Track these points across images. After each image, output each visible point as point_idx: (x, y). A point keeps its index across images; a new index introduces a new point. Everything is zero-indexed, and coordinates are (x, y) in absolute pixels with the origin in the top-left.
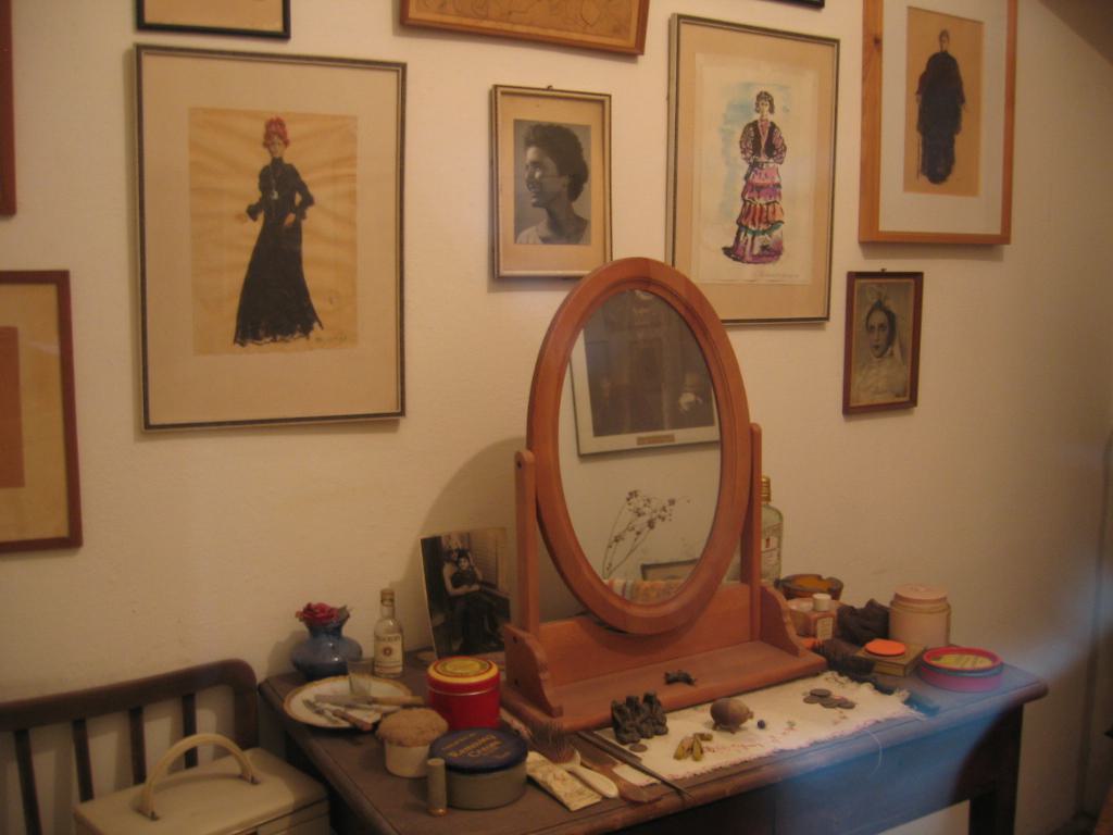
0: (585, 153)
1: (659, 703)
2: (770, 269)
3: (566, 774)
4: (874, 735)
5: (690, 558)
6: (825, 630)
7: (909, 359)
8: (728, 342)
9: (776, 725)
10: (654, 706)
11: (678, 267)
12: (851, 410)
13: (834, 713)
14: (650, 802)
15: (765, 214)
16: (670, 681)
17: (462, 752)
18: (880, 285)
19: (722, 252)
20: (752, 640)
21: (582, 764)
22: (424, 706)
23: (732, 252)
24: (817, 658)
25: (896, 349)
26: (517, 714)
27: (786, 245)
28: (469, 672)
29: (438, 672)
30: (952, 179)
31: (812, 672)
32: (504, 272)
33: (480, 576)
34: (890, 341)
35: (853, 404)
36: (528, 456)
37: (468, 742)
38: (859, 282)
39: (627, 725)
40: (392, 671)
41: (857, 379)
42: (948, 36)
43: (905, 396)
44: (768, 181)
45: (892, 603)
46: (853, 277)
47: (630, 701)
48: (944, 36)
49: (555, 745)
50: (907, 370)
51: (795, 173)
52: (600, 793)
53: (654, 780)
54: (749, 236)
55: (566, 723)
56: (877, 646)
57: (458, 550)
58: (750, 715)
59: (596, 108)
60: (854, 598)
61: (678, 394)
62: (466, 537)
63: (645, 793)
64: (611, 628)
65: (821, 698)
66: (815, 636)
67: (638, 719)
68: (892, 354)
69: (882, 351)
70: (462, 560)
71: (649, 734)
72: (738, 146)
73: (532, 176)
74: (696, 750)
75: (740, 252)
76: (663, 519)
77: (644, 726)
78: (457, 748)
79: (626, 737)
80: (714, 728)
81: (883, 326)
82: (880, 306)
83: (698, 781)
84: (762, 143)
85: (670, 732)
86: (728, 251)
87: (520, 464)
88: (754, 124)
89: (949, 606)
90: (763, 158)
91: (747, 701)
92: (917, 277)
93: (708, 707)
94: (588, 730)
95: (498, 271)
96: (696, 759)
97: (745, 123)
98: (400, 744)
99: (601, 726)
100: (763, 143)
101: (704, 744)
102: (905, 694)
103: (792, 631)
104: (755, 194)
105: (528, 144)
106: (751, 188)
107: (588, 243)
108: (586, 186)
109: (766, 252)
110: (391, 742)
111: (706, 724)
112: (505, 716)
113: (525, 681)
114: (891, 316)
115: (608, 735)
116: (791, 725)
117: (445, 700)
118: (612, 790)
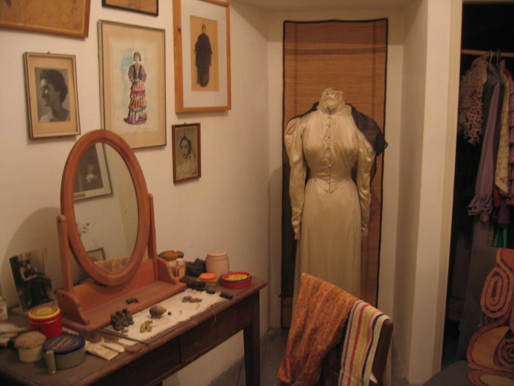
0: (66, 82)
1: (129, 312)
2: (142, 126)
3: (101, 347)
4: (212, 310)
5: (97, 248)
6: (182, 273)
7: (197, 157)
8: (135, 159)
9: (175, 313)
10: (127, 314)
11: (107, 128)
12: (176, 181)
13: (195, 304)
14: (138, 351)
15: (139, 103)
16: (129, 302)
17: (58, 346)
18: (184, 130)
19: (123, 121)
20: (155, 281)
21: (105, 342)
22: (30, 331)
23: (128, 120)
24: (183, 284)
25: (192, 155)
26: (69, 327)
27: (148, 116)
28: (47, 312)
29: (34, 315)
30: (209, 85)
31: (182, 290)
32: (35, 136)
33: (37, 271)
34: (189, 152)
35: (177, 179)
36: (63, 217)
37: (59, 342)
38: (177, 129)
39: (118, 323)
40: (4, 319)
41: (178, 169)
42: (205, 27)
43: (196, 173)
44: (140, 90)
45: (206, 258)
46: (174, 127)
47: (118, 313)
48: (203, 27)
49: (94, 336)
50: (196, 163)
51: (149, 85)
52: (117, 351)
53: (136, 342)
54: (134, 113)
55: (93, 326)
56: (203, 276)
57: (25, 261)
58: (165, 311)
59: (69, 62)
60: (190, 258)
61: (86, 174)
62: (29, 255)
63: (135, 347)
64: (102, 285)
65: (188, 299)
66: (178, 275)
67: (121, 320)
68: (190, 157)
69: (186, 157)
70: (28, 265)
71: (127, 324)
72: (128, 75)
73: (44, 92)
74: (148, 328)
75: (131, 120)
76: (85, 232)
77: (125, 323)
78: (55, 345)
79: (119, 328)
80: (152, 318)
81: (186, 144)
82: (184, 138)
83: (153, 339)
84: (136, 74)
85: (135, 323)
86: (126, 120)
87: (59, 221)
88: (134, 66)
89: (228, 257)
90: (138, 80)
91: (163, 305)
92: (198, 125)
93: (148, 310)
94: (102, 328)
95: (33, 135)
96: (149, 331)
97: (130, 66)
98: (28, 348)
99: (106, 325)
100: (137, 73)
101: (151, 325)
102: (219, 293)
103: (171, 275)
104: (135, 95)
105: (41, 78)
106: (133, 93)
107: (70, 120)
108: (67, 96)
109: (141, 119)
110: (23, 348)
111: (148, 317)
112: (64, 329)
113: (70, 312)
114: (189, 143)
115: (110, 328)
116: (181, 312)
117: (38, 326)
118: (122, 350)
